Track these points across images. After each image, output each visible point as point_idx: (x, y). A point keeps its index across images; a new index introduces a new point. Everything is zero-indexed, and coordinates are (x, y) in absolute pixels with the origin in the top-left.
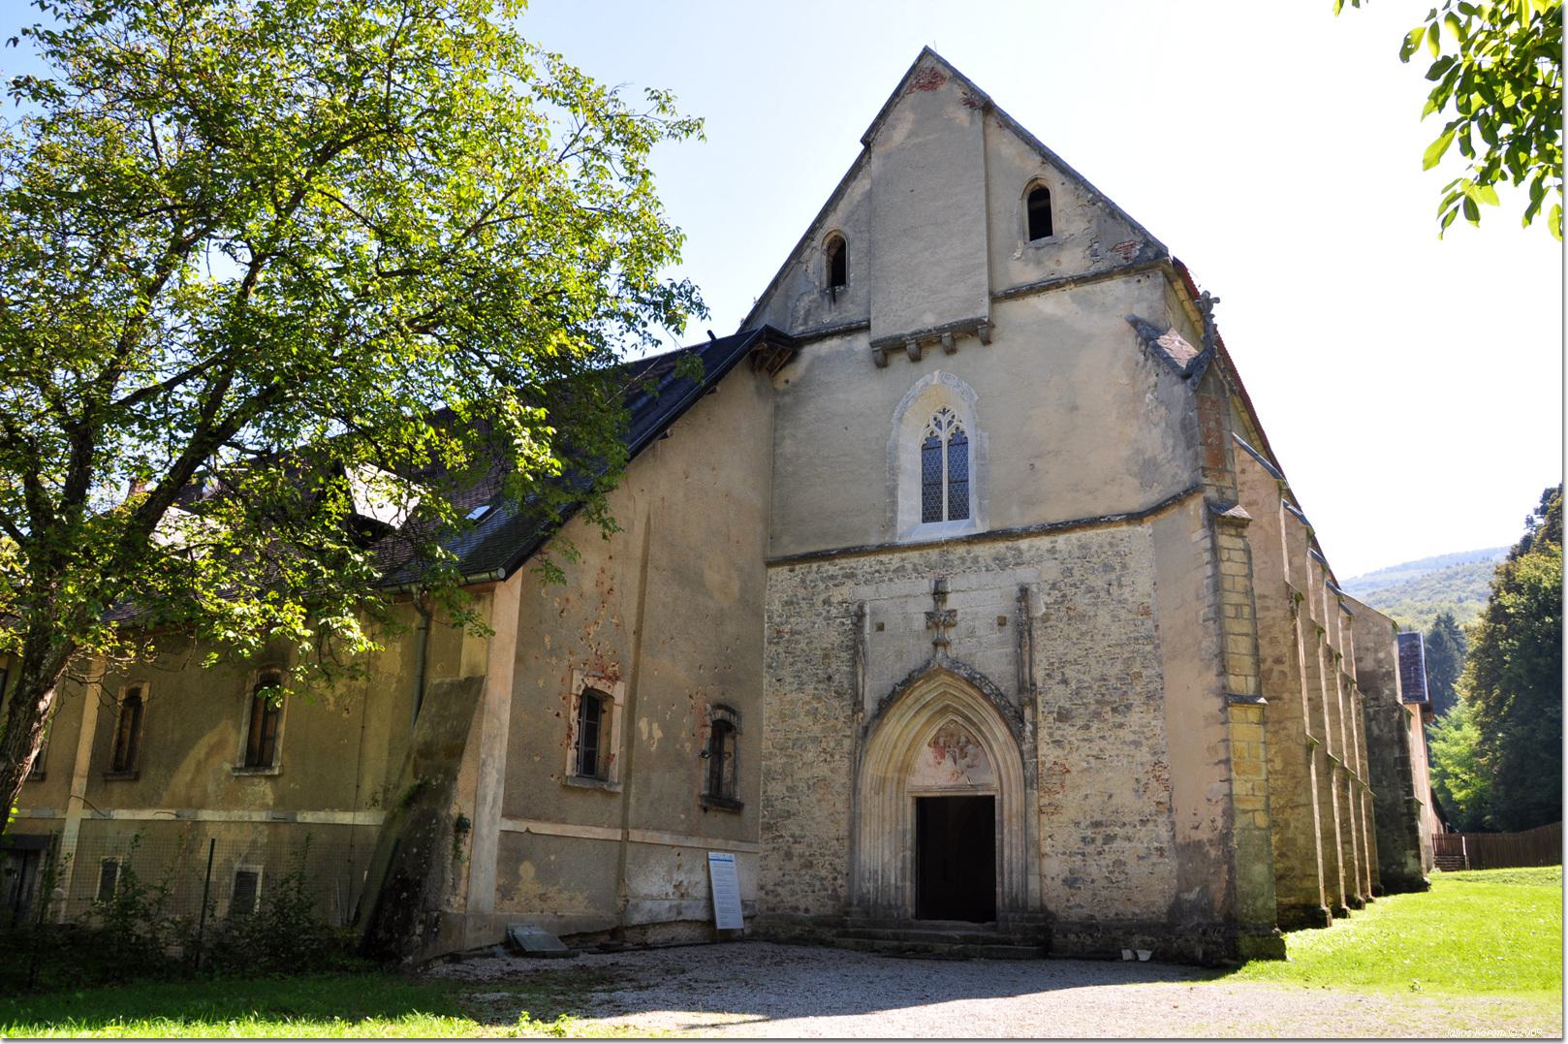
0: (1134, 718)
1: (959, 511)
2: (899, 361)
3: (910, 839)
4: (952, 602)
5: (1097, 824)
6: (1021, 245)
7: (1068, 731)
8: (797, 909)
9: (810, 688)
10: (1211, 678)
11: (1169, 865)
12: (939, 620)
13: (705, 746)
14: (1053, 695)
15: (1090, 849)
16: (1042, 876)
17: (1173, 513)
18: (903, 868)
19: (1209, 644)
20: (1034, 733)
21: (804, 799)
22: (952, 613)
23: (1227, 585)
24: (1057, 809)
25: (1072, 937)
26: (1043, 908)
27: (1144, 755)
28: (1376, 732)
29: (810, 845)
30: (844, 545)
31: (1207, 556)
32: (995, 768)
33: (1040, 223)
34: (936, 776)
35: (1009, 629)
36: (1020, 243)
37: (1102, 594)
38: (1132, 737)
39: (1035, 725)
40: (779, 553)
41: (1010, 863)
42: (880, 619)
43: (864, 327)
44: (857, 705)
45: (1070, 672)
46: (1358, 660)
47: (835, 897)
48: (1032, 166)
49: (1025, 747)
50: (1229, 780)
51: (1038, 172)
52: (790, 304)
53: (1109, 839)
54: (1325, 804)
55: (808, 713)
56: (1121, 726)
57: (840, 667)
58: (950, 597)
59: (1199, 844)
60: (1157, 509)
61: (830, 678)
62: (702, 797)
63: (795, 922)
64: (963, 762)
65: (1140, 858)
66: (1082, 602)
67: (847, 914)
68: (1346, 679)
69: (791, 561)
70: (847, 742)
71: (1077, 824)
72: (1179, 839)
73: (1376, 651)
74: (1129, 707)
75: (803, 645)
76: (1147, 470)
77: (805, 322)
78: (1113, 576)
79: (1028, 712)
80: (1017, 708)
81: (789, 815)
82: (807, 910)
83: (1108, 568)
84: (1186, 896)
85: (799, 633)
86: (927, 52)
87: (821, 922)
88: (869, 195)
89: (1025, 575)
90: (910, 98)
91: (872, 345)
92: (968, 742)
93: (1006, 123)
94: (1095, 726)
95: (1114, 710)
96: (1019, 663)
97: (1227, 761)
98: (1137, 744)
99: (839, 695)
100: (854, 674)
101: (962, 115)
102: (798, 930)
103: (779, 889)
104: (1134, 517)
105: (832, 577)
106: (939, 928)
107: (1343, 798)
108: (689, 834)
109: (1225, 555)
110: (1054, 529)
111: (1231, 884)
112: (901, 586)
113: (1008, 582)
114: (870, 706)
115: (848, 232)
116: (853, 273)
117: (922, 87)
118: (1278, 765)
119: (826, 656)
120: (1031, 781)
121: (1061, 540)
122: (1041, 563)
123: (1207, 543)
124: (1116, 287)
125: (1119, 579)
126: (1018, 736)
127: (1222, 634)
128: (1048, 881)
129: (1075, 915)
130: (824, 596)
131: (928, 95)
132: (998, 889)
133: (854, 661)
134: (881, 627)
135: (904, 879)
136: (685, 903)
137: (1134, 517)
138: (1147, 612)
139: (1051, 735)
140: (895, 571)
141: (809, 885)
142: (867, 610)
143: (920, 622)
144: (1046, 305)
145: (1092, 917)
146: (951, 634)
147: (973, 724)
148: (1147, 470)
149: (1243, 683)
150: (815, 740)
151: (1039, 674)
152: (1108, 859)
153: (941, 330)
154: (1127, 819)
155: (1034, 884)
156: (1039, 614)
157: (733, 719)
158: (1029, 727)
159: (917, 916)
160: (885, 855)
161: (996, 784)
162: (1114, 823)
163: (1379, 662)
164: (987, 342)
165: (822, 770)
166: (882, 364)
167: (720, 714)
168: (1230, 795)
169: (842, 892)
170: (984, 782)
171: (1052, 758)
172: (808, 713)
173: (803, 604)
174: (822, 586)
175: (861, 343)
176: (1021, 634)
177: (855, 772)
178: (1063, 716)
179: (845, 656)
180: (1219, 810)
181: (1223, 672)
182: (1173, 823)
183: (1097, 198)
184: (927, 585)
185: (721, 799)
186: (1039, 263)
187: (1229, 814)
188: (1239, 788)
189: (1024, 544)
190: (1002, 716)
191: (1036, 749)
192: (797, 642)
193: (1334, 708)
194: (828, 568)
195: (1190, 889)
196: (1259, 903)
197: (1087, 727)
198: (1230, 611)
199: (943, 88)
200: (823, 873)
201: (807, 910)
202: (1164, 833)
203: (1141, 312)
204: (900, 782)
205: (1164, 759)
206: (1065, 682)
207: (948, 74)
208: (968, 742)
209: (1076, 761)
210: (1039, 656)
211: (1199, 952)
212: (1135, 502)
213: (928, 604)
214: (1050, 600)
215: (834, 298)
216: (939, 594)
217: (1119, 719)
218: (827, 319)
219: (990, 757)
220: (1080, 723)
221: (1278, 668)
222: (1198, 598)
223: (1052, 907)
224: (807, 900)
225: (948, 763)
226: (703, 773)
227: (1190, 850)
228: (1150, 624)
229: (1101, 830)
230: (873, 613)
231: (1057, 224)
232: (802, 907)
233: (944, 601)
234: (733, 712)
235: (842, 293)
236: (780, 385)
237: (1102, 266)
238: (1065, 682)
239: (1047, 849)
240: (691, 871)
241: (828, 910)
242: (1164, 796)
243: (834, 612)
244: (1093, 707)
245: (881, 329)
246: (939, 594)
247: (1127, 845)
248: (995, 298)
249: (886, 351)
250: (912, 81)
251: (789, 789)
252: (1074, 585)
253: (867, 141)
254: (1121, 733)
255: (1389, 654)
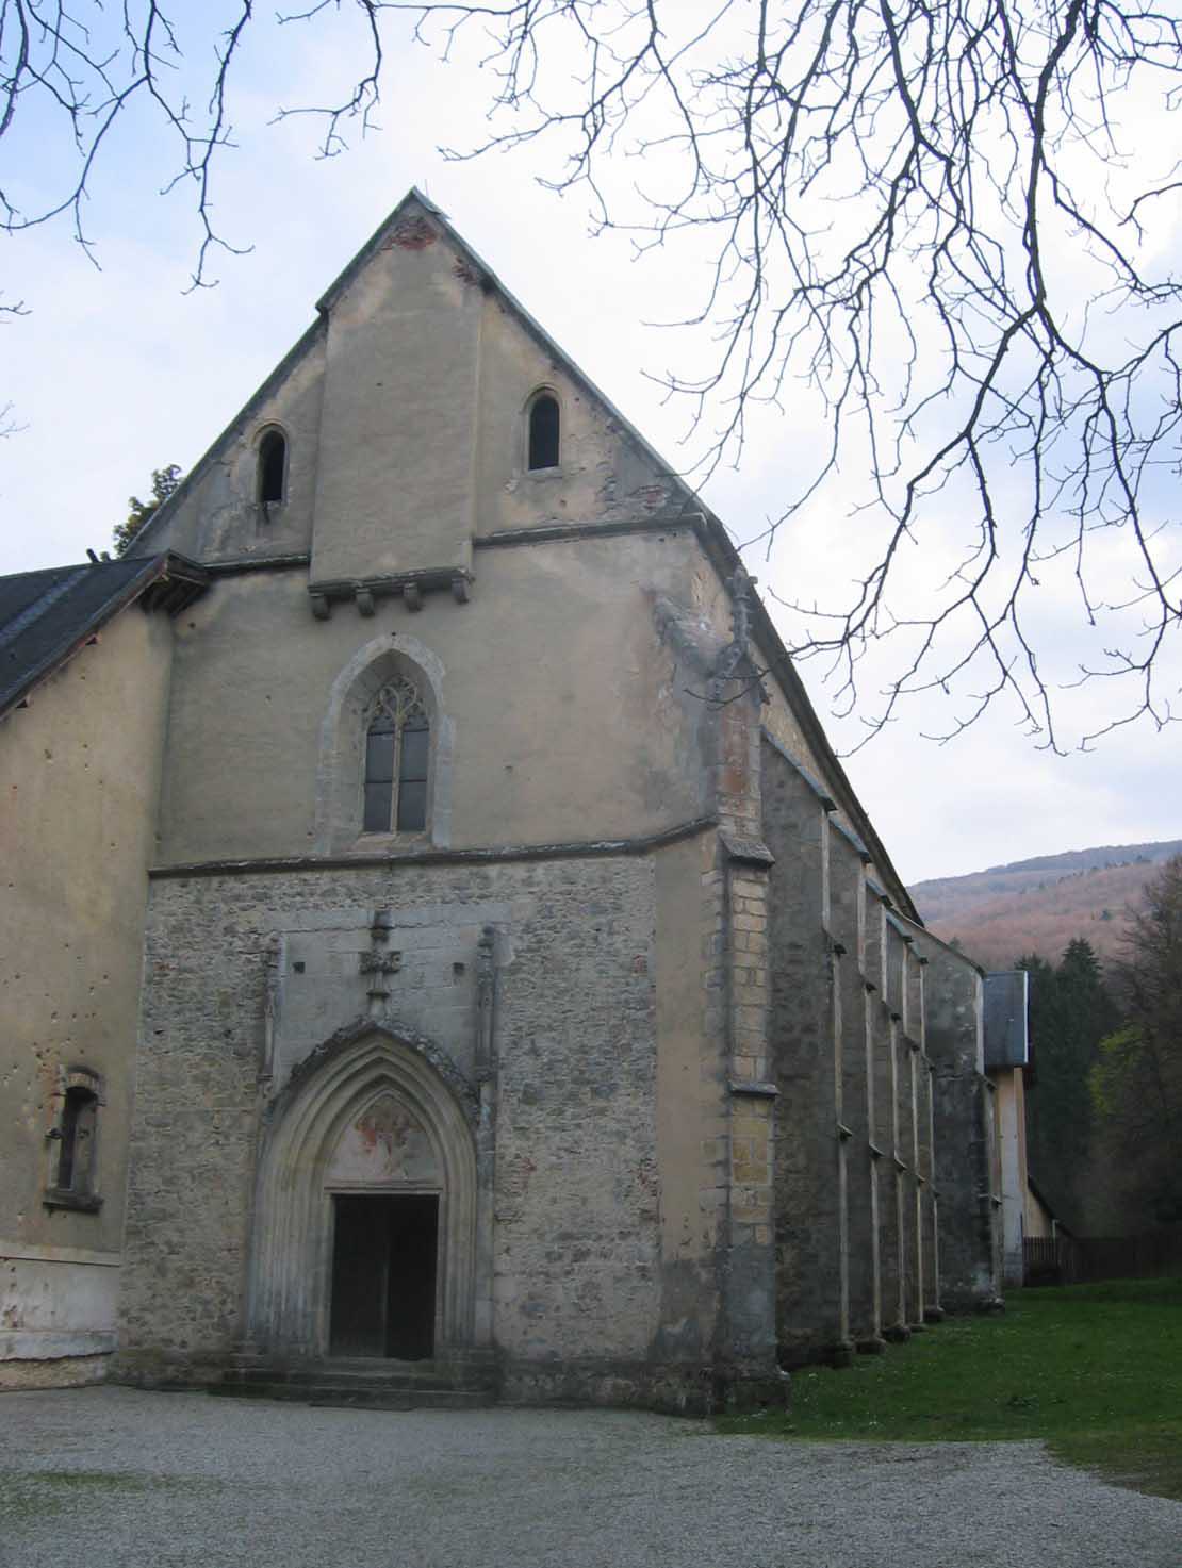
0: (621, 1103)
1: (413, 821)
2: (345, 617)
3: (325, 1250)
4: (396, 940)
5: (565, 1236)
6: (519, 472)
7: (537, 1117)
8: (169, 1342)
9: (201, 1047)
10: (713, 1060)
11: (651, 1295)
12: (377, 967)
13: (56, 1123)
14: (521, 1068)
15: (556, 1268)
16: (493, 1300)
17: (684, 847)
18: (315, 1289)
19: (712, 1015)
20: (493, 1117)
21: (188, 1196)
22: (394, 955)
23: (739, 943)
24: (516, 1218)
25: (528, 1379)
26: (494, 1343)
27: (629, 1150)
28: (948, 1109)
29: (191, 1257)
30: (259, 855)
31: (717, 906)
32: (440, 1166)
33: (544, 445)
34: (362, 1166)
35: (467, 979)
36: (516, 472)
37: (589, 943)
38: (614, 1126)
39: (494, 1107)
40: (168, 863)
41: (454, 1280)
42: (299, 958)
43: (303, 564)
44: (264, 1077)
45: (543, 1042)
46: (931, 1015)
47: (222, 1325)
48: (539, 373)
49: (480, 1135)
50: (727, 1187)
51: (547, 379)
52: (203, 520)
53: (581, 1255)
54: (860, 1208)
55: (196, 1079)
56: (602, 1112)
57: (242, 1019)
58: (394, 935)
59: (686, 1266)
60: (663, 841)
61: (228, 1033)
62: (47, 1192)
63: (167, 1361)
64: (399, 1152)
65: (618, 1280)
66: (562, 949)
67: (238, 1349)
68: (908, 1046)
69: (183, 874)
70: (248, 1120)
71: (541, 1236)
72: (665, 1257)
73: (955, 1004)
74: (613, 1088)
75: (194, 988)
76: (654, 786)
77: (222, 548)
78: (603, 919)
79: (485, 1091)
80: (474, 1084)
81: (164, 1216)
82: (184, 1344)
83: (598, 909)
84: (669, 1328)
85: (190, 971)
86: (413, 198)
87: (202, 1360)
88: (320, 382)
89: (492, 911)
90: (388, 256)
91: (312, 589)
92: (407, 1124)
93: (510, 307)
94: (569, 1112)
95: (596, 1092)
96: (477, 1023)
97: (725, 1164)
98: (621, 1136)
99: (241, 1056)
100: (261, 1029)
101: (452, 289)
102: (170, 1371)
103: (148, 1317)
104: (635, 849)
105: (238, 898)
106: (363, 1368)
107: (889, 1199)
108: (30, 1241)
109: (739, 906)
110: (532, 856)
111: (722, 1319)
112: (333, 916)
113: (472, 921)
114: (280, 1073)
115: (292, 431)
116: (292, 486)
117: (405, 242)
118: (801, 1161)
119: (225, 1004)
120: (487, 1179)
121: (540, 870)
122: (512, 898)
123: (718, 888)
124: (634, 547)
125: (610, 924)
126: (473, 1123)
127: (728, 1006)
128: (501, 1307)
129: (536, 1350)
130: (224, 923)
131: (410, 256)
132: (438, 1318)
133: (261, 1013)
134: (299, 967)
135: (315, 1301)
136: (18, 1335)
137: (635, 849)
138: (642, 968)
139: (514, 1121)
140: (323, 895)
141: (188, 1310)
142: (283, 945)
143: (352, 966)
144: (544, 559)
145: (554, 1354)
146: (392, 984)
147: (416, 1102)
148: (654, 786)
149: (753, 1069)
150: (205, 1116)
151: (503, 1040)
152: (578, 1281)
153: (406, 579)
154: (603, 1231)
155: (482, 1309)
156: (506, 964)
157: (94, 1086)
158: (486, 1110)
159: (332, 1352)
160: (291, 1271)
161: (441, 1182)
162: (587, 1236)
163: (957, 1018)
164: (462, 600)
165: (212, 1155)
166: (321, 616)
167: (77, 1079)
168: (727, 1205)
169: (233, 1321)
170: (424, 1176)
171: (513, 1150)
172: (196, 1079)
173: (197, 931)
174: (224, 908)
175: (296, 584)
176: (482, 989)
177: (257, 1161)
178: (530, 1097)
179: (251, 1004)
180: (712, 1223)
181: (728, 1052)
182: (659, 1237)
183: (617, 427)
184: (364, 916)
185: (72, 1199)
186: (537, 501)
187: (725, 1229)
188: (738, 1197)
189: (493, 871)
190: (453, 1096)
191: (493, 1137)
192: (186, 982)
193: (884, 1083)
194: (233, 885)
195: (675, 1321)
196: (756, 1339)
197: (561, 1113)
198: (740, 976)
199: (433, 248)
200: (208, 1294)
201: (184, 1344)
202: (648, 1249)
203: (661, 579)
204: (316, 1175)
205: (653, 1155)
206: (535, 1052)
207: (439, 231)
208: (407, 1124)
209: (543, 1156)
210: (504, 1018)
211: (682, 1401)
212: (642, 825)
213: (363, 941)
214: (520, 945)
215: (266, 518)
216: (380, 931)
217: (600, 1103)
218: (253, 545)
219: (433, 1139)
220: (551, 1105)
221: (807, 1039)
222: (703, 956)
223: (504, 1341)
224: (185, 1332)
225: (380, 1150)
226: (52, 1159)
227: (679, 1270)
228: (645, 984)
229: (572, 1245)
230: (291, 949)
231: (568, 451)
232: (177, 1340)
233: (385, 939)
234: (95, 1076)
235: (277, 511)
236: (184, 631)
237: (618, 516)
238: (535, 1052)
239: (501, 1267)
240: (27, 1292)
241: (213, 1344)
242: (647, 1202)
243: (238, 944)
244: (569, 1086)
245: (325, 569)
246: (380, 931)
247: (600, 1262)
248: (479, 545)
249: (331, 600)
250: (391, 232)
251: (169, 1181)
252: (552, 928)
253: (324, 307)
254: (602, 1121)
255: (970, 1009)
